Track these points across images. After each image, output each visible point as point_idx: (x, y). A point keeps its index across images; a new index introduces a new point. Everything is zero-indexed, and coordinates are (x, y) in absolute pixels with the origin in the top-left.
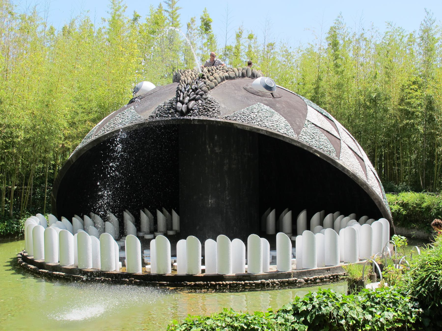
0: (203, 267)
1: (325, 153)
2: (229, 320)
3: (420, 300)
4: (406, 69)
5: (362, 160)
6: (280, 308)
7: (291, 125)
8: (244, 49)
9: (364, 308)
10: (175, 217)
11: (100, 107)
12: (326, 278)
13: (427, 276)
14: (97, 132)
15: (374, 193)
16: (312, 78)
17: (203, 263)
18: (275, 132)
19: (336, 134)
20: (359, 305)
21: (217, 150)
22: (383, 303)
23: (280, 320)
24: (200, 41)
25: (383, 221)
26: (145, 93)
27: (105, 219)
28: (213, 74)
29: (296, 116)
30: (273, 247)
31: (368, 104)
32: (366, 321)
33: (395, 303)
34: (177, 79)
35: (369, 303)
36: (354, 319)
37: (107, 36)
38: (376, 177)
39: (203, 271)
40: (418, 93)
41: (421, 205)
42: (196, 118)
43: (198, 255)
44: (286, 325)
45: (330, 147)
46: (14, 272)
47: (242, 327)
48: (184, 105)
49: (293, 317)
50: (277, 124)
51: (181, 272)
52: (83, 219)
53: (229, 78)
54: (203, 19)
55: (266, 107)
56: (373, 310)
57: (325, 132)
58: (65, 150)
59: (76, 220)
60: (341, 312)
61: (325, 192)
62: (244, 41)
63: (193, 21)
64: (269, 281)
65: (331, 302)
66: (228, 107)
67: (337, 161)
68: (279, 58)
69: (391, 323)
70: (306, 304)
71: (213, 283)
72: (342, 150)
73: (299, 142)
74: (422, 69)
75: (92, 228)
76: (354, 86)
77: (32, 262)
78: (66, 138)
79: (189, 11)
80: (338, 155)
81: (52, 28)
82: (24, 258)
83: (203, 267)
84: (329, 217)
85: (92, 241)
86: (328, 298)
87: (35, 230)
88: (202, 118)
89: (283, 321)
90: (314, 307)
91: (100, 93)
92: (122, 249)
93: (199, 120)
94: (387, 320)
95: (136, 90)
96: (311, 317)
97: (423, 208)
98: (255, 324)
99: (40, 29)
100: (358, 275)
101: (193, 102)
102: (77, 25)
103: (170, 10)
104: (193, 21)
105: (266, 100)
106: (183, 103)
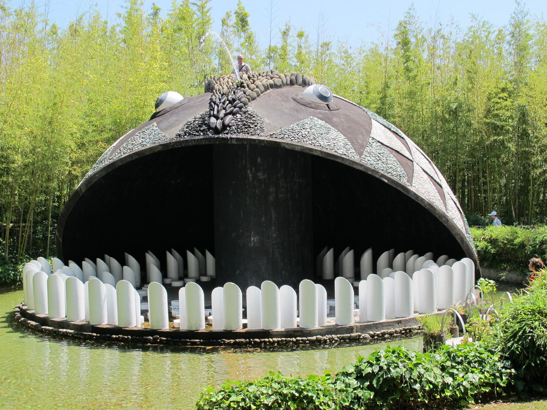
0: (245, 321)
1: (395, 178)
2: (276, 386)
7: (352, 143)
9: (443, 369)
10: (210, 259)
12: (396, 332)
15: (454, 227)
17: (245, 316)
19: (407, 154)
21: (261, 176)
23: (340, 386)
25: (466, 261)
28: (254, 81)
29: (358, 133)
30: (331, 295)
31: (447, 116)
32: (446, 386)
33: (481, 362)
34: (209, 88)
35: (449, 363)
36: (431, 383)
39: (245, 326)
40: (508, 103)
41: (513, 241)
42: (234, 136)
44: (347, 391)
45: (400, 170)
46: (10, 329)
47: (293, 395)
48: (219, 121)
49: (355, 382)
51: (218, 327)
55: (320, 122)
56: (455, 371)
58: (72, 178)
59: (87, 264)
60: (415, 374)
61: (390, 224)
62: (293, 41)
65: (401, 362)
66: (273, 122)
69: (476, 387)
70: (371, 365)
72: (415, 175)
75: (107, 275)
76: (429, 95)
77: (33, 317)
80: (410, 181)
81: (54, 26)
82: (23, 313)
83: (245, 321)
84: (399, 257)
86: (398, 357)
87: (36, 277)
88: (241, 136)
89: (343, 386)
90: (381, 368)
91: (116, 105)
92: (144, 299)
93: (238, 139)
94: (472, 384)
96: (378, 381)
97: (515, 245)
99: (39, 27)
100: (435, 329)
102: (85, 22)
105: (320, 113)
106: (217, 118)
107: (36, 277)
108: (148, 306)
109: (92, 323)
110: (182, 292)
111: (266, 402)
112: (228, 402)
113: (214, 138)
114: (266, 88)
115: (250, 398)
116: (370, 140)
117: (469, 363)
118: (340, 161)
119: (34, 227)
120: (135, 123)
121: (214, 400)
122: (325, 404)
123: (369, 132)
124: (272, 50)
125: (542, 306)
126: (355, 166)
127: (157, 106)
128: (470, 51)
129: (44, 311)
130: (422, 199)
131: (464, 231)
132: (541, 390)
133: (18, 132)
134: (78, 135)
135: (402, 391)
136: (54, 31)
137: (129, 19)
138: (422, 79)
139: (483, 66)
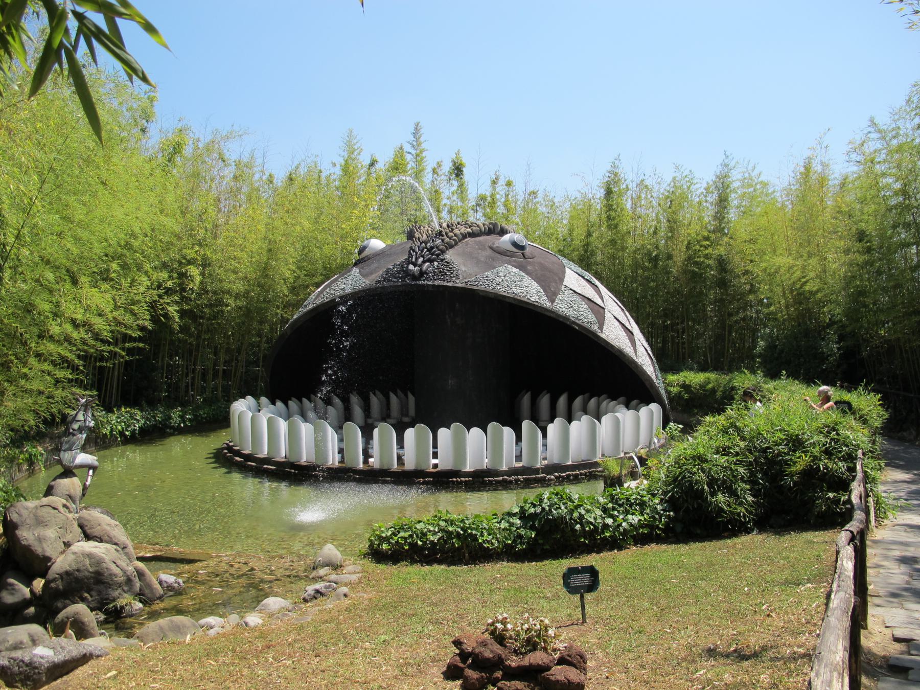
0: (435, 461)
2: (443, 524)
3: (672, 503)
7: (545, 291)
8: (500, 198)
9: (605, 510)
12: (581, 474)
13: (680, 473)
14: (316, 298)
15: (644, 373)
16: (580, 234)
17: (435, 456)
19: (599, 301)
23: (504, 525)
24: (448, 190)
25: (654, 407)
29: (551, 281)
30: (519, 439)
32: (606, 526)
33: (642, 505)
34: (410, 236)
35: (610, 505)
36: (591, 523)
37: (337, 183)
39: (436, 466)
40: (710, 251)
41: (705, 387)
42: (430, 283)
44: (510, 530)
45: (591, 317)
46: (216, 465)
47: (458, 533)
49: (518, 522)
50: (530, 290)
51: (410, 464)
54: (454, 163)
55: (514, 270)
56: (616, 513)
58: (284, 321)
59: (293, 404)
60: (576, 515)
61: (575, 369)
62: (501, 188)
63: (439, 165)
64: (512, 478)
65: (564, 504)
66: (466, 269)
72: (606, 322)
73: (554, 312)
75: (311, 415)
77: (238, 453)
80: (601, 328)
81: (270, 176)
82: (230, 449)
83: (435, 461)
84: (593, 401)
85: (306, 429)
86: (561, 499)
87: (240, 415)
88: (436, 283)
90: (543, 509)
92: (341, 440)
93: (434, 286)
94: (631, 525)
95: (361, 251)
96: (540, 521)
99: (257, 177)
100: (615, 471)
103: (413, 152)
104: (439, 165)
105: (515, 261)
106: (415, 265)
107: (240, 415)
108: (344, 445)
109: (292, 460)
111: (432, 538)
112: (396, 538)
113: (411, 285)
114: (464, 236)
117: (631, 505)
120: (343, 269)
121: (384, 535)
122: (488, 542)
123: (562, 280)
124: (483, 198)
126: (546, 313)
127: (360, 252)
128: (675, 201)
132: (699, 531)
133: (232, 277)
136: (270, 180)
137: (346, 170)
138: (623, 228)
139: (685, 216)
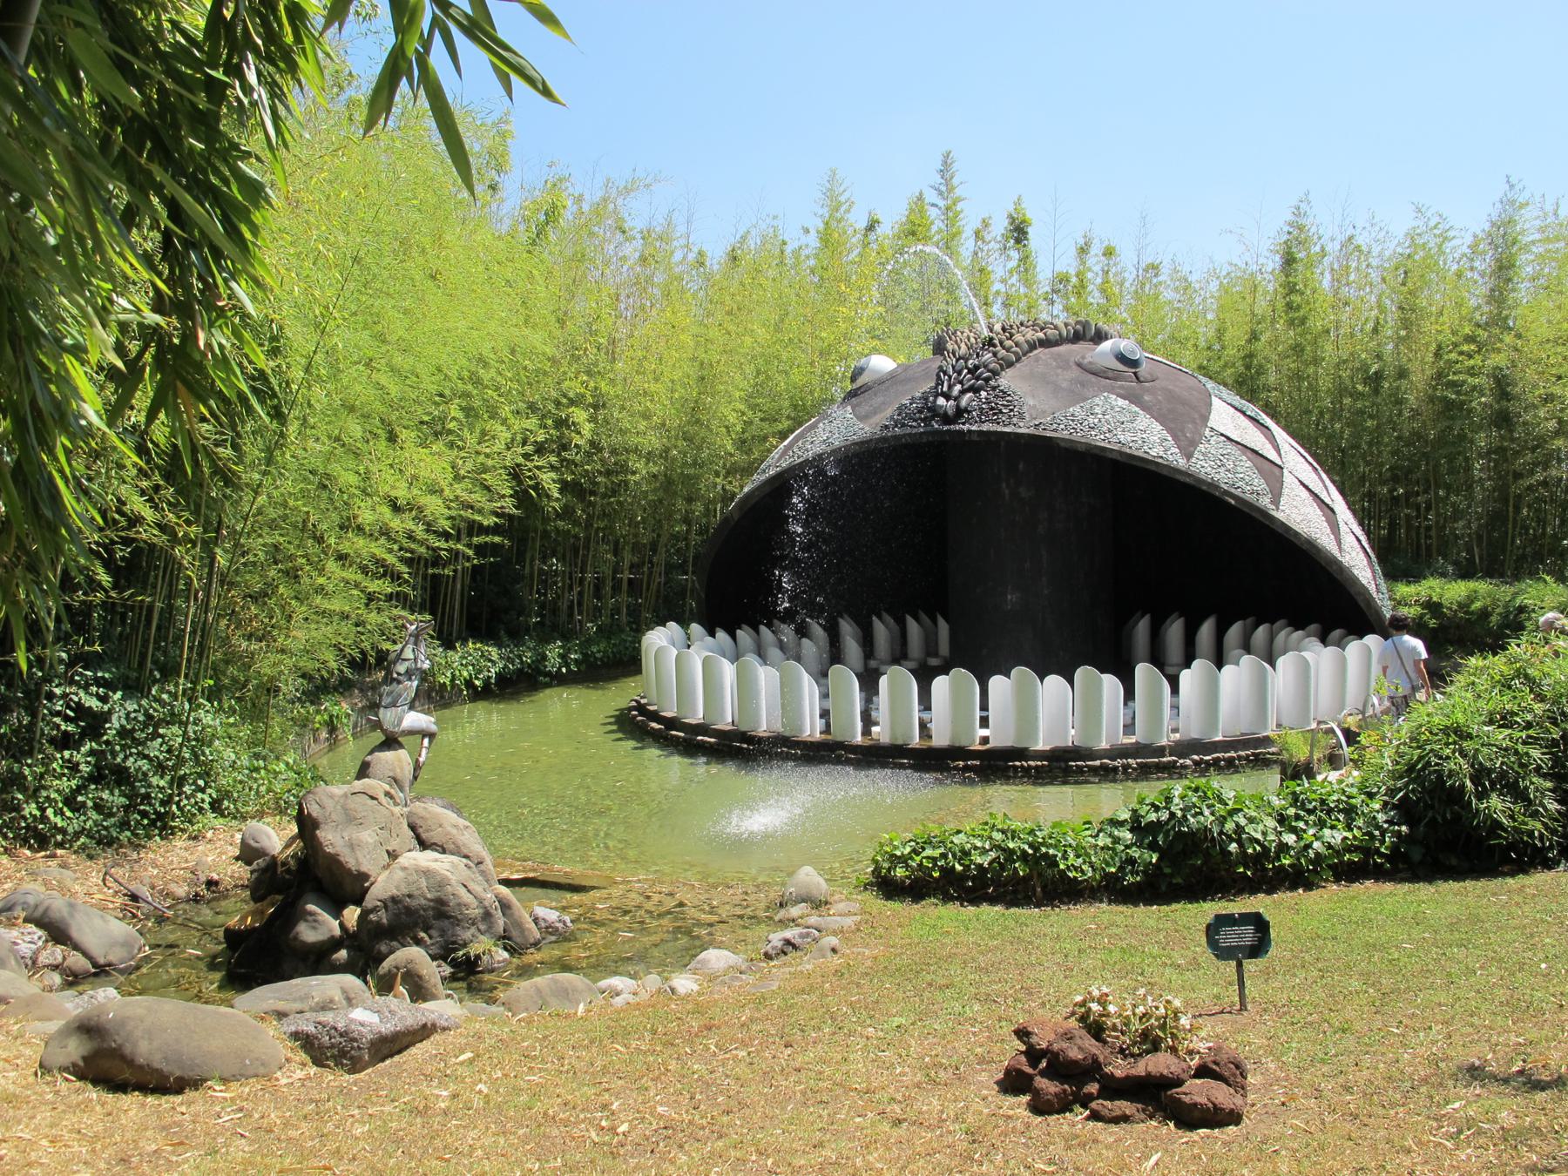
0: (985, 732)
1: (1247, 497)
2: (998, 836)
3: (1405, 810)
4: (1454, 305)
5: (1332, 510)
6: (1107, 814)
7: (1175, 438)
8: (1094, 279)
9: (1282, 819)
10: (943, 627)
11: (795, 407)
12: (1239, 758)
13: (1421, 758)
14: (777, 460)
15: (1355, 581)
16: (1236, 336)
17: (984, 722)
18: (1140, 453)
19: (1272, 455)
20: (1270, 815)
21: (1024, 492)
22: (1324, 812)
23: (1103, 840)
24: (1001, 267)
26: (876, 376)
27: (802, 631)
28: (1012, 335)
29: (1185, 420)
30: (1129, 694)
31: (1360, 388)
32: (1283, 848)
33: (1350, 811)
34: (939, 348)
35: (1292, 811)
36: (1257, 841)
37: (812, 262)
38: (1363, 547)
39: (985, 740)
40: (1476, 361)
41: (1468, 606)
43: (973, 711)
44: (1113, 849)
45: (1259, 483)
47: (1024, 852)
48: (951, 402)
49: (1129, 836)
50: (1147, 437)
51: (940, 739)
52: (757, 632)
53: (1046, 343)
54: (1012, 219)
55: (1121, 402)
56: (1301, 824)
57: (1249, 453)
58: (727, 497)
60: (1229, 826)
61: (1242, 578)
62: (1095, 261)
63: (986, 224)
65: (1209, 807)
66: (1037, 403)
67: (1274, 513)
68: (1168, 295)
69: (1338, 852)
70: (1157, 809)
71: (997, 765)
72: (1285, 491)
74: (1486, 309)
75: (774, 653)
76: (1328, 350)
77: (655, 716)
78: (728, 473)
79: (984, 207)
80: (1276, 501)
82: (641, 708)
83: (985, 732)
84: (1261, 632)
85: (766, 677)
86: (1204, 798)
87: (659, 652)
88: (985, 427)
89: (1108, 841)
90: (1172, 815)
91: (798, 376)
92: (825, 696)
93: (981, 433)
94: (1330, 847)
96: (1167, 834)
97: (1472, 613)
98: (1049, 846)
99: (678, 256)
100: (1300, 752)
101: (969, 395)
102: (752, 243)
103: (941, 203)
104: (986, 224)
105: (1122, 387)
106: (947, 397)
107: (659, 652)
108: (829, 704)
110: (883, 681)
112: (918, 859)
115: (954, 856)
116: (1207, 432)
117: (1329, 811)
118: (1153, 468)
119: (666, 574)
121: (898, 853)
122: (1076, 869)
123: (1205, 418)
124: (1063, 279)
125: (1462, 721)
127: (853, 379)
128: (1412, 272)
129: (695, 712)
130: (1296, 533)
131: (1372, 588)
132: (1454, 862)
133: (642, 425)
134: (739, 428)
135: (1207, 855)
137: (825, 238)
138: (1316, 324)
139: (1432, 299)
